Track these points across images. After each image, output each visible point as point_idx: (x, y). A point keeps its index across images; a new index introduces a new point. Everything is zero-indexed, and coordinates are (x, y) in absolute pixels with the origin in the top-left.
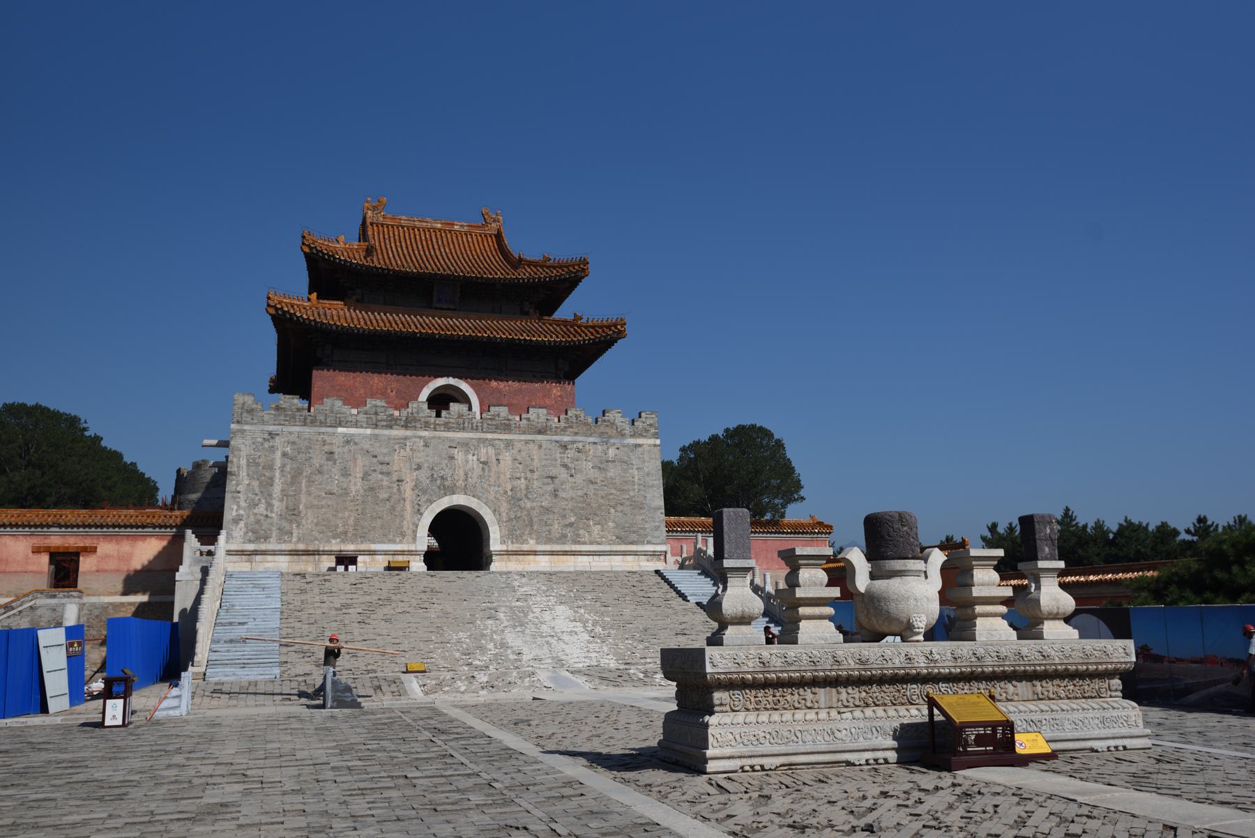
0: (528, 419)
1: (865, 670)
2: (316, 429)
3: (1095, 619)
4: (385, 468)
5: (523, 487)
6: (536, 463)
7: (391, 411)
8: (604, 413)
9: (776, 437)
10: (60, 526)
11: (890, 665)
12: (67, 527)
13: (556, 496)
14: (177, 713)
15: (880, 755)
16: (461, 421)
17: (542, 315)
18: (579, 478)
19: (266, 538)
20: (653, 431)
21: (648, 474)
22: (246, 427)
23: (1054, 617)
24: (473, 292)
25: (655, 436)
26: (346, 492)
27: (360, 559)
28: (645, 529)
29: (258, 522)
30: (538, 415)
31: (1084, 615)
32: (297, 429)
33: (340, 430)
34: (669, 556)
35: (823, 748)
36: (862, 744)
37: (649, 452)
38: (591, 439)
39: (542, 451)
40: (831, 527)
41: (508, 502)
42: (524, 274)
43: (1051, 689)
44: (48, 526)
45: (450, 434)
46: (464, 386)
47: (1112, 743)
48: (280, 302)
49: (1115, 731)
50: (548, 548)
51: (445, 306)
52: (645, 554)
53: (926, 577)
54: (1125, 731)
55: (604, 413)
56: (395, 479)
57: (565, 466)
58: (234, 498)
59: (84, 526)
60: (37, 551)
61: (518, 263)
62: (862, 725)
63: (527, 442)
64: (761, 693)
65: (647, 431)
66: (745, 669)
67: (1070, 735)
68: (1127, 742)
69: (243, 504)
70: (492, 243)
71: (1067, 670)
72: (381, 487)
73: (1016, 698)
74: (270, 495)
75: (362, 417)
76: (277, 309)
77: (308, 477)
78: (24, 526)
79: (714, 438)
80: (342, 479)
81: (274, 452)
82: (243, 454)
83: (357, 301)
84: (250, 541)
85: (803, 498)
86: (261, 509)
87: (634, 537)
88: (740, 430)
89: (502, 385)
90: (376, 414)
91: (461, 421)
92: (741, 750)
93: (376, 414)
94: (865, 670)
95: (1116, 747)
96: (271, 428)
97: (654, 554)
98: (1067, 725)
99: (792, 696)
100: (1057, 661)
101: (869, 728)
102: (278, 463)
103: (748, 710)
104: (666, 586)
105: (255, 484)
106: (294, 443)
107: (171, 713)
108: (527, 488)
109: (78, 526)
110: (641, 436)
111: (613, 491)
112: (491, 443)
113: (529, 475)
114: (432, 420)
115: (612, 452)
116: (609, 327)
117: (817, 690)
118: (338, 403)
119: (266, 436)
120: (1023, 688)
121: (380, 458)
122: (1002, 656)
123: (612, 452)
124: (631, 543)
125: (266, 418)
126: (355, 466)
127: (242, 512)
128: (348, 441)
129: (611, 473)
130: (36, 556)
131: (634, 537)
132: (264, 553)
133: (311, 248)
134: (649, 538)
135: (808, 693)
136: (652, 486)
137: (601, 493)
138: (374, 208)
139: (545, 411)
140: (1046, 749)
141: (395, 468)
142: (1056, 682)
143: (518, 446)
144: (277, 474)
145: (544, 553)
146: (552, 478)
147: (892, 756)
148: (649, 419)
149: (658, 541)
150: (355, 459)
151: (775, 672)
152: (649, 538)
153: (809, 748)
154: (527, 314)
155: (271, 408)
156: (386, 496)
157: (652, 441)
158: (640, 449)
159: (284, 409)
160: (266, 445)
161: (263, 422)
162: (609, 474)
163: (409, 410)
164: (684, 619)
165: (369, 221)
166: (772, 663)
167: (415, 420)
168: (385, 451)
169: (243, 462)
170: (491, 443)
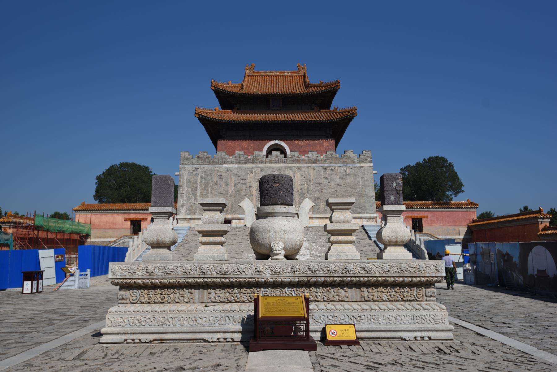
0: (308, 157)
1: (223, 278)
2: (214, 166)
3: (544, 248)
4: (244, 182)
5: (306, 188)
6: (312, 177)
7: (246, 156)
8: (345, 152)
9: (449, 161)
10: (134, 210)
11: (243, 275)
12: (136, 210)
13: (322, 192)
14: (73, 288)
15: (228, 335)
16: (277, 159)
17: (320, 109)
18: (333, 183)
19: (195, 213)
20: (369, 159)
21: (367, 180)
22: (186, 166)
23: (396, 244)
24: (288, 101)
25: (370, 162)
26: (227, 192)
27: (233, 221)
28: (365, 206)
29: (191, 206)
30: (312, 155)
31: (539, 247)
32: (206, 166)
33: (224, 165)
34: (378, 219)
35: (186, 330)
36: (217, 327)
37: (367, 170)
38: (338, 165)
39: (315, 171)
40: (477, 205)
41: (299, 195)
42: (311, 90)
43: (376, 294)
44: (130, 210)
45: (272, 165)
46: (283, 144)
47: (419, 334)
48: (201, 112)
49: (421, 326)
50: (318, 216)
51: (276, 109)
52: (366, 218)
53: (298, 217)
54: (430, 326)
55: (345, 152)
56: (248, 186)
57: (326, 178)
58: (182, 196)
59: (142, 210)
60: (126, 220)
61: (307, 86)
62: (218, 315)
63: (307, 167)
64: (152, 292)
65: (366, 160)
66: (136, 276)
67: (382, 327)
68: (431, 334)
69: (185, 199)
70: (301, 79)
71: (386, 281)
72: (242, 190)
73: (347, 299)
74: (196, 195)
75: (234, 160)
76: (199, 115)
77: (211, 186)
78: (121, 210)
79: (418, 164)
80: (226, 187)
81: (197, 176)
82: (185, 177)
83: (238, 109)
84: (188, 214)
85: (463, 191)
86: (192, 200)
87: (360, 210)
88: (431, 159)
89: (300, 142)
90: (240, 158)
91: (277, 159)
92: (128, 329)
93: (240, 158)
94: (223, 278)
95: (422, 338)
96: (196, 166)
97: (370, 218)
98: (382, 320)
99: (176, 294)
100: (377, 274)
101: (227, 316)
102: (199, 181)
103: (142, 303)
104: (364, 233)
105: (190, 190)
106: (205, 172)
107: (70, 288)
108: (308, 189)
109: (140, 210)
110: (363, 162)
111: (349, 189)
112: (291, 168)
113: (309, 183)
114: (264, 159)
115: (348, 171)
116: (348, 112)
117: (193, 291)
118: (224, 154)
119: (194, 169)
120: (353, 293)
121: (242, 177)
122: (331, 270)
123: (348, 171)
124: (359, 213)
125: (194, 161)
126: (231, 181)
127: (184, 202)
128: (228, 170)
129: (348, 180)
130: (126, 222)
131: (360, 210)
132: (194, 219)
133: (215, 88)
134: (367, 211)
135: (186, 293)
136: (369, 186)
137: (343, 190)
138: (250, 69)
139: (316, 153)
140: (352, 336)
141: (248, 181)
142: (380, 289)
143: (303, 169)
144: (199, 186)
145: (316, 218)
146: (320, 184)
147: (238, 337)
148: (367, 154)
149: (372, 212)
150: (231, 178)
151: (157, 278)
152: (367, 211)
153: (175, 330)
154: (313, 109)
155: (195, 157)
156: (244, 194)
157: (368, 165)
158: (362, 169)
159: (201, 157)
160: (194, 173)
161: (193, 164)
162: (347, 181)
163: (254, 155)
164: (363, 249)
165: (246, 74)
166: (155, 273)
167: (257, 160)
168: (244, 174)
169: (185, 181)
170: (291, 168)
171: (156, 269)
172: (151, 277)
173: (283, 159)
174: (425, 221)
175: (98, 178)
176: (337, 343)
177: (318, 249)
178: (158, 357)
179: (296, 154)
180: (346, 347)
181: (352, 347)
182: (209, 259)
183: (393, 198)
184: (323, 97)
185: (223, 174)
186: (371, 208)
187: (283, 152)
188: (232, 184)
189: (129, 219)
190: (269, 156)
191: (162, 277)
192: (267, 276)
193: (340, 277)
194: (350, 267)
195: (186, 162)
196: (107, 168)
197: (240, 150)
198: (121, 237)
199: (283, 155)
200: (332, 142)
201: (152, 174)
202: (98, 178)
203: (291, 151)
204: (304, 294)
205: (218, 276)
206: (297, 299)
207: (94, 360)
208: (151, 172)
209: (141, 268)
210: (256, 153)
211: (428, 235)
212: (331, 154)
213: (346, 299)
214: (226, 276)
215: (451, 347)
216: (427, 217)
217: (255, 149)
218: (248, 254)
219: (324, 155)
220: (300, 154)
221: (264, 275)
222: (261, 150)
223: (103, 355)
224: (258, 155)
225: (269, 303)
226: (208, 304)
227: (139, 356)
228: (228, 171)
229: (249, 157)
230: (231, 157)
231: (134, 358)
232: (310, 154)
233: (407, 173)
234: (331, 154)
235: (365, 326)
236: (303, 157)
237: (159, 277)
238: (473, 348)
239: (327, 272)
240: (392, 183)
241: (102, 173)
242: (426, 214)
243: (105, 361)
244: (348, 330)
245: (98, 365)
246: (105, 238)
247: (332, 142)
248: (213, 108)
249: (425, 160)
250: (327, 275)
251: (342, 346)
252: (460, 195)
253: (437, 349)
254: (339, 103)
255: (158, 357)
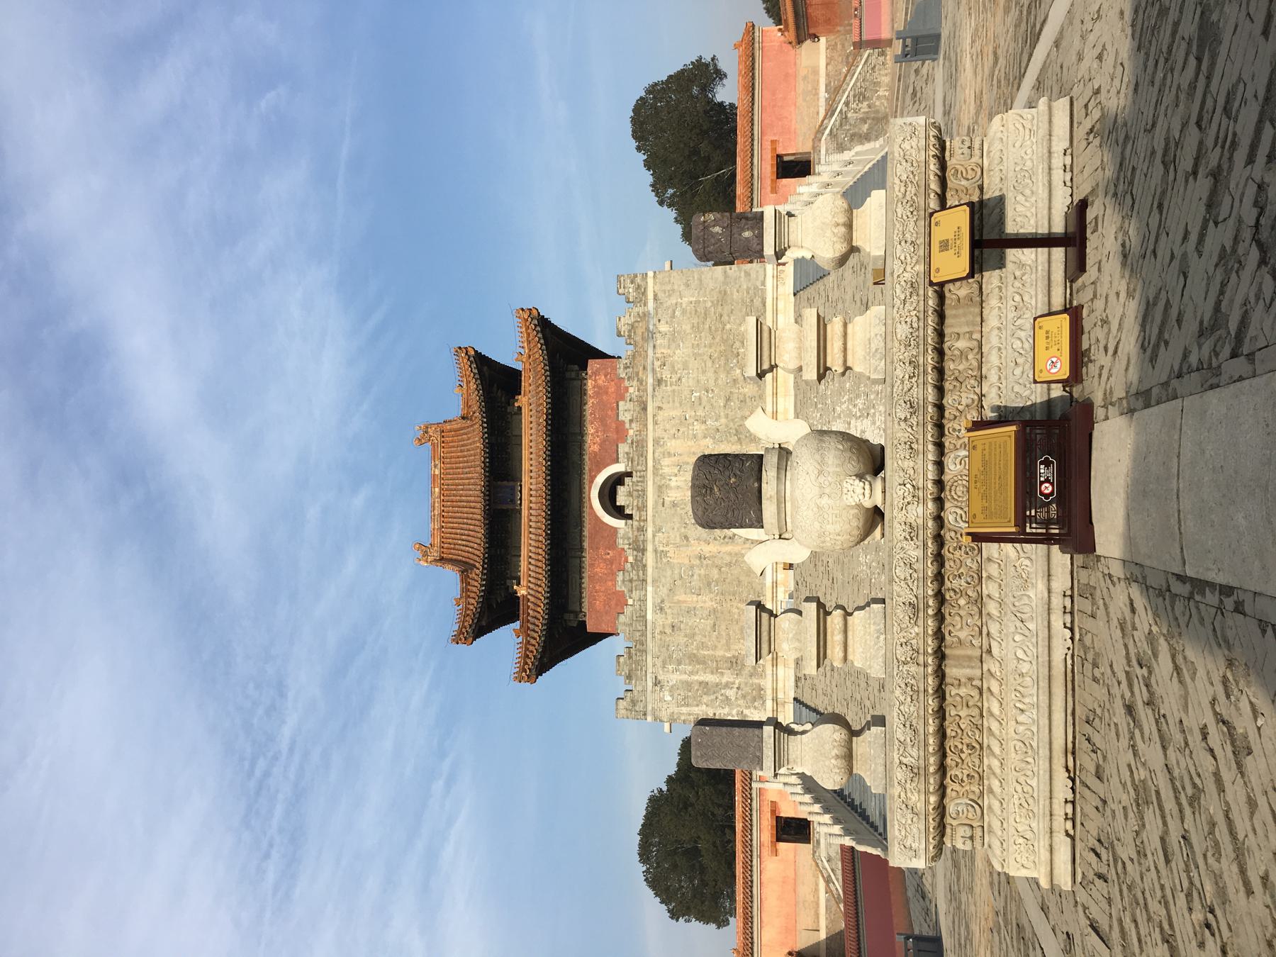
0: (631, 421)
11: (919, 566)
16: (635, 494)
22: (649, 708)
29: (744, 697)
30: (626, 411)
33: (649, 617)
35: (1044, 698)
37: (662, 284)
46: (600, 479)
60: (776, 853)
63: (656, 423)
74: (717, 685)
75: (636, 594)
79: (648, 165)
82: (676, 710)
84: (764, 702)
85: (713, 59)
86: (731, 693)
87: (757, 302)
90: (631, 581)
91: (635, 494)
96: (650, 684)
101: (1026, 580)
105: (705, 699)
110: (644, 293)
114: (635, 524)
118: (622, 618)
123: (663, 328)
125: (640, 688)
131: (757, 302)
132: (775, 690)
134: (759, 284)
139: (621, 403)
141: (687, 562)
143: (659, 433)
145: (775, 403)
150: (679, 602)
152: (759, 284)
156: (715, 571)
158: (660, 295)
161: (644, 691)
168: (669, 573)
169: (684, 710)
171: (905, 761)
172: (922, 772)
173: (635, 479)
174: (784, 148)
175: (674, 915)
176: (1078, 358)
177: (850, 400)
178: (1105, 758)
179: (623, 448)
180: (1085, 337)
181: (1087, 324)
182: (882, 643)
183: (747, 234)
184: (496, 383)
185: (670, 621)
186: (753, 275)
187: (618, 480)
188: (691, 599)
189: (774, 845)
190: (628, 511)
191: (922, 749)
192: (921, 513)
193: (926, 351)
194: (902, 331)
195: (640, 707)
196: (651, 893)
197: (614, 580)
198: (817, 865)
199: (627, 480)
200: (593, 365)
201: (665, 788)
202: (674, 915)
203: (617, 461)
204: (963, 431)
205: (920, 622)
206: (974, 448)
207: (1109, 901)
208: (661, 791)
209: (903, 795)
210: (621, 543)
211: (817, 139)
212: (626, 368)
213: (975, 336)
214: (921, 606)
215: (1086, 106)
216: (773, 142)
217: (613, 545)
218: (860, 564)
219: (627, 383)
220: (624, 441)
221: (920, 522)
222: (615, 531)
223: (1098, 882)
224: (625, 537)
225: (984, 509)
226: (985, 647)
227: (1105, 802)
228: (661, 609)
229: (631, 559)
230: (630, 602)
231: (1108, 812)
232: (625, 417)
233: (671, 191)
234: (626, 368)
235: (1040, 297)
236: (631, 432)
237: (922, 753)
238: (1089, 55)
239: (914, 380)
240: (713, 235)
241: (664, 907)
242: (768, 146)
243: (1112, 875)
244: (1047, 332)
245: (1121, 891)
246: (818, 904)
247: (593, 365)
248: (505, 642)
249: (639, 149)
250: (921, 381)
251: (1085, 346)
252: (722, 65)
253: (1091, 136)
254: (511, 348)
255: (1105, 758)
